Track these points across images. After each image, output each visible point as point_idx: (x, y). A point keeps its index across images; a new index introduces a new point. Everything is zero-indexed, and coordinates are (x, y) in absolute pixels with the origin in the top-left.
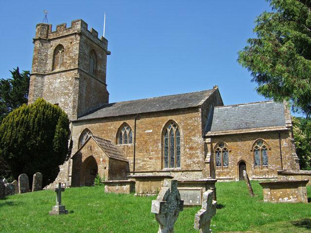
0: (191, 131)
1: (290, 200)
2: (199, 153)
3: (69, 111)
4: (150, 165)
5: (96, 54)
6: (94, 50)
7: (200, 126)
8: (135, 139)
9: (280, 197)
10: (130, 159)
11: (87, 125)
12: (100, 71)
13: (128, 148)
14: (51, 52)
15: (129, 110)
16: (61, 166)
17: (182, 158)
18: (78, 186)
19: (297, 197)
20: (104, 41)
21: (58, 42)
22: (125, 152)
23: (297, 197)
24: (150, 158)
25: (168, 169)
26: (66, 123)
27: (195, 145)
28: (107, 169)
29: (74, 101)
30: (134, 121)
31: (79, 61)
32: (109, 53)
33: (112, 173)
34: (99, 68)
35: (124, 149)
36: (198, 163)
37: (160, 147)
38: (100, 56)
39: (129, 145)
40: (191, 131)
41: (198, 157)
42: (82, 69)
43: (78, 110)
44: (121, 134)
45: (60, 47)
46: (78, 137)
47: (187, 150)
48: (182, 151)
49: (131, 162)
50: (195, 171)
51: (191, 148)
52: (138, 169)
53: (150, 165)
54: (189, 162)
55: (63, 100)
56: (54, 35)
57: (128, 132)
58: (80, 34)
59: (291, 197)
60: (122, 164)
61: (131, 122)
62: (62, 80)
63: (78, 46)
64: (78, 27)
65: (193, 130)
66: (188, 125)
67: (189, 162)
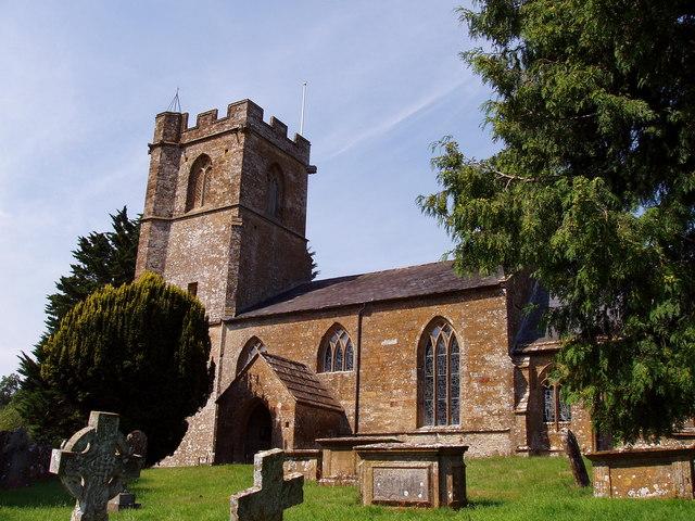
0: (482, 341)
1: (654, 494)
2: (504, 392)
3: (214, 302)
4: (391, 418)
5: (283, 175)
6: (277, 164)
7: (505, 329)
8: (359, 359)
9: (630, 488)
10: (348, 406)
11: (253, 329)
12: (292, 210)
13: (345, 380)
14: (184, 170)
15: (350, 295)
16: (189, 419)
17: (463, 403)
18: (230, 461)
19: (669, 487)
20: (302, 144)
21: (199, 150)
22: (336, 383)
23: (669, 487)
24: (392, 404)
25: (433, 428)
26: (202, 326)
27: (492, 374)
28: (292, 426)
29: (229, 278)
30: (356, 317)
31: (242, 190)
32: (313, 170)
33: (304, 435)
34: (289, 204)
35: (334, 383)
36: (499, 415)
37: (414, 378)
38: (293, 178)
39: (347, 373)
40: (482, 341)
41: (499, 401)
42: (250, 207)
43: (237, 296)
44: (329, 348)
45: (203, 159)
46: (237, 356)
47: (475, 385)
48: (463, 389)
49: (350, 412)
50: (491, 432)
51: (484, 381)
52: (365, 429)
53: (391, 418)
54: (478, 411)
55: (207, 275)
56: (191, 135)
57: (344, 343)
58: (245, 131)
59: (656, 486)
60: (328, 416)
61: (350, 322)
62: (205, 232)
63: (240, 158)
64: (243, 115)
65: (489, 339)
66: (477, 327)
67: (478, 411)
